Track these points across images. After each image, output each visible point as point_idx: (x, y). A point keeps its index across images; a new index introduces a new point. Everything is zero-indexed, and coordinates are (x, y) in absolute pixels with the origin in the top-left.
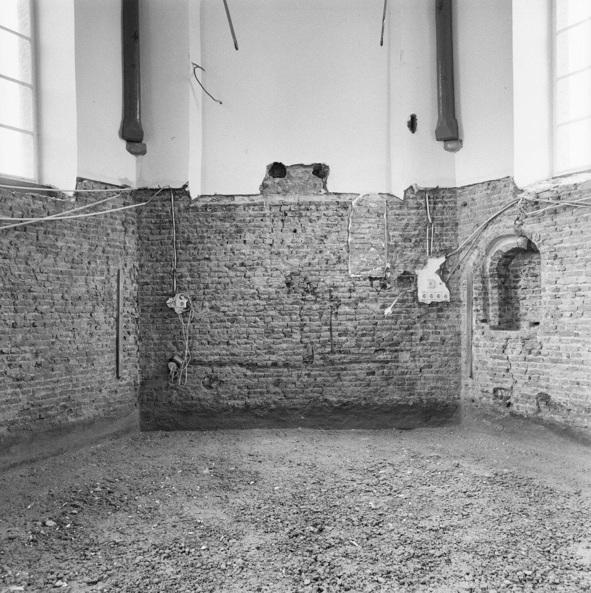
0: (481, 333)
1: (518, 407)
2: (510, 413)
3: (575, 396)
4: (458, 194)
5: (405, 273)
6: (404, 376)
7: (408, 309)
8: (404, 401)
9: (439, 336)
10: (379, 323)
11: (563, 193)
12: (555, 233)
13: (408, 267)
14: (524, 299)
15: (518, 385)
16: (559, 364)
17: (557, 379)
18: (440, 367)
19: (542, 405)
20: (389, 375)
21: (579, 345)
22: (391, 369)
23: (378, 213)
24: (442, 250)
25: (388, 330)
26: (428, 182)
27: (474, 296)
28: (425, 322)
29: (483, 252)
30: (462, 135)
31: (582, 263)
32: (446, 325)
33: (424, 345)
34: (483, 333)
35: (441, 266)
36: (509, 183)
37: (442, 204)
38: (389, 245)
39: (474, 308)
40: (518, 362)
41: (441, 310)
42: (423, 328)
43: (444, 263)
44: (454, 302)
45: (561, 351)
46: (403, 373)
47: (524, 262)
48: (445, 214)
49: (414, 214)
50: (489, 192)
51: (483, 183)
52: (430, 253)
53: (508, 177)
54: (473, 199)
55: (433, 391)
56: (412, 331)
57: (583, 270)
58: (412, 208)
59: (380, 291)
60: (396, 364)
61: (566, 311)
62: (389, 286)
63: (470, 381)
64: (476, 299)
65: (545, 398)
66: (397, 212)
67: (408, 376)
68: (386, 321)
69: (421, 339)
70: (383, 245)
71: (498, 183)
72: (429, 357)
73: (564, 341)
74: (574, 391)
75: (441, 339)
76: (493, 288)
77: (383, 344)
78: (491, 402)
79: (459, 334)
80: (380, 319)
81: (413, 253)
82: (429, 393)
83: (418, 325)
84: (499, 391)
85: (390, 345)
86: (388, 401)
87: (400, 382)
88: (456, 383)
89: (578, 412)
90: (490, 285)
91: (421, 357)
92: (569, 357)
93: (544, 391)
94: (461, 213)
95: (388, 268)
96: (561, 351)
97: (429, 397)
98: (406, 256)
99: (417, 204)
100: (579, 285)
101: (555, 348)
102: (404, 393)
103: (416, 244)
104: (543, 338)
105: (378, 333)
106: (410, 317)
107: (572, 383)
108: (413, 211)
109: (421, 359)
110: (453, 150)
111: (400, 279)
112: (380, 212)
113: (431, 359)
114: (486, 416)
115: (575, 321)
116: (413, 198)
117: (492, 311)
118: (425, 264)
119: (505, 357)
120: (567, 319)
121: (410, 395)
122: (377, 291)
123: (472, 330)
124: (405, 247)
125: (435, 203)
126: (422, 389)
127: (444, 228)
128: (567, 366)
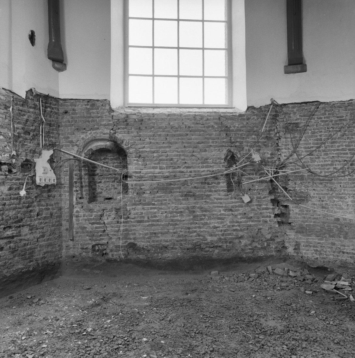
0: (81, 207)
1: (112, 255)
2: (106, 260)
3: (153, 241)
4: (60, 104)
5: (27, 160)
6: (26, 247)
7: (28, 191)
8: (27, 268)
9: (49, 212)
10: (7, 204)
11: (145, 118)
12: (140, 142)
13: (28, 156)
14: (100, 182)
15: (112, 240)
16: (142, 224)
17: (141, 232)
18: (50, 235)
19: (130, 251)
20: (15, 248)
21: (156, 210)
22: (16, 242)
23: (6, 105)
24: (50, 145)
25: (14, 209)
26: (43, 89)
27: (75, 180)
28: (39, 201)
29: (81, 149)
30: (67, 61)
31: (157, 162)
32: (53, 203)
33: (39, 219)
34: (82, 207)
35: (50, 157)
36: (106, 104)
37: (50, 108)
38: (14, 135)
39: (74, 189)
40: (112, 225)
41: (49, 191)
42: (38, 205)
43: (52, 155)
44: (58, 185)
45: (143, 215)
46: (25, 245)
47: (101, 158)
48: (52, 117)
49: (33, 113)
50: (88, 107)
51: (84, 100)
52: (42, 145)
53: (106, 100)
54: (73, 110)
55: (46, 255)
56: (30, 209)
57: (158, 166)
58: (31, 107)
59: (7, 175)
60: (20, 238)
61: (146, 190)
62: (14, 171)
63: (71, 243)
64: (76, 182)
65: (133, 246)
66: (21, 108)
67: (29, 247)
68: (12, 201)
69: (38, 215)
70: (10, 134)
71: (96, 102)
72: (43, 228)
73: (146, 209)
74: (153, 239)
75: (50, 213)
76: (85, 174)
77: (10, 221)
78: (90, 255)
79: (60, 209)
80: (8, 200)
81: (32, 145)
82: (43, 257)
83: (35, 204)
84: (97, 246)
85: (15, 222)
86: (15, 271)
87: (23, 253)
88: (59, 246)
89: (155, 251)
90: (83, 173)
91: (37, 229)
92: (148, 218)
93: (132, 241)
94: (62, 118)
95: (14, 155)
96: (143, 215)
97: (43, 260)
98: (26, 147)
99: (34, 105)
100: (155, 175)
101: (140, 213)
102: (26, 261)
103: (33, 137)
104: (131, 207)
105: (7, 212)
106: (30, 197)
107: (151, 233)
108: (31, 110)
109: (37, 231)
110: (59, 70)
111: (22, 166)
112: (8, 105)
113: (44, 230)
114: (85, 266)
115: (153, 196)
116: (31, 99)
117: (85, 191)
118: (40, 154)
119: (102, 222)
120: (147, 195)
121: (31, 261)
122: (6, 175)
123: (73, 205)
124: (26, 139)
125: (46, 107)
126: (38, 255)
127: (51, 128)
128: (148, 224)
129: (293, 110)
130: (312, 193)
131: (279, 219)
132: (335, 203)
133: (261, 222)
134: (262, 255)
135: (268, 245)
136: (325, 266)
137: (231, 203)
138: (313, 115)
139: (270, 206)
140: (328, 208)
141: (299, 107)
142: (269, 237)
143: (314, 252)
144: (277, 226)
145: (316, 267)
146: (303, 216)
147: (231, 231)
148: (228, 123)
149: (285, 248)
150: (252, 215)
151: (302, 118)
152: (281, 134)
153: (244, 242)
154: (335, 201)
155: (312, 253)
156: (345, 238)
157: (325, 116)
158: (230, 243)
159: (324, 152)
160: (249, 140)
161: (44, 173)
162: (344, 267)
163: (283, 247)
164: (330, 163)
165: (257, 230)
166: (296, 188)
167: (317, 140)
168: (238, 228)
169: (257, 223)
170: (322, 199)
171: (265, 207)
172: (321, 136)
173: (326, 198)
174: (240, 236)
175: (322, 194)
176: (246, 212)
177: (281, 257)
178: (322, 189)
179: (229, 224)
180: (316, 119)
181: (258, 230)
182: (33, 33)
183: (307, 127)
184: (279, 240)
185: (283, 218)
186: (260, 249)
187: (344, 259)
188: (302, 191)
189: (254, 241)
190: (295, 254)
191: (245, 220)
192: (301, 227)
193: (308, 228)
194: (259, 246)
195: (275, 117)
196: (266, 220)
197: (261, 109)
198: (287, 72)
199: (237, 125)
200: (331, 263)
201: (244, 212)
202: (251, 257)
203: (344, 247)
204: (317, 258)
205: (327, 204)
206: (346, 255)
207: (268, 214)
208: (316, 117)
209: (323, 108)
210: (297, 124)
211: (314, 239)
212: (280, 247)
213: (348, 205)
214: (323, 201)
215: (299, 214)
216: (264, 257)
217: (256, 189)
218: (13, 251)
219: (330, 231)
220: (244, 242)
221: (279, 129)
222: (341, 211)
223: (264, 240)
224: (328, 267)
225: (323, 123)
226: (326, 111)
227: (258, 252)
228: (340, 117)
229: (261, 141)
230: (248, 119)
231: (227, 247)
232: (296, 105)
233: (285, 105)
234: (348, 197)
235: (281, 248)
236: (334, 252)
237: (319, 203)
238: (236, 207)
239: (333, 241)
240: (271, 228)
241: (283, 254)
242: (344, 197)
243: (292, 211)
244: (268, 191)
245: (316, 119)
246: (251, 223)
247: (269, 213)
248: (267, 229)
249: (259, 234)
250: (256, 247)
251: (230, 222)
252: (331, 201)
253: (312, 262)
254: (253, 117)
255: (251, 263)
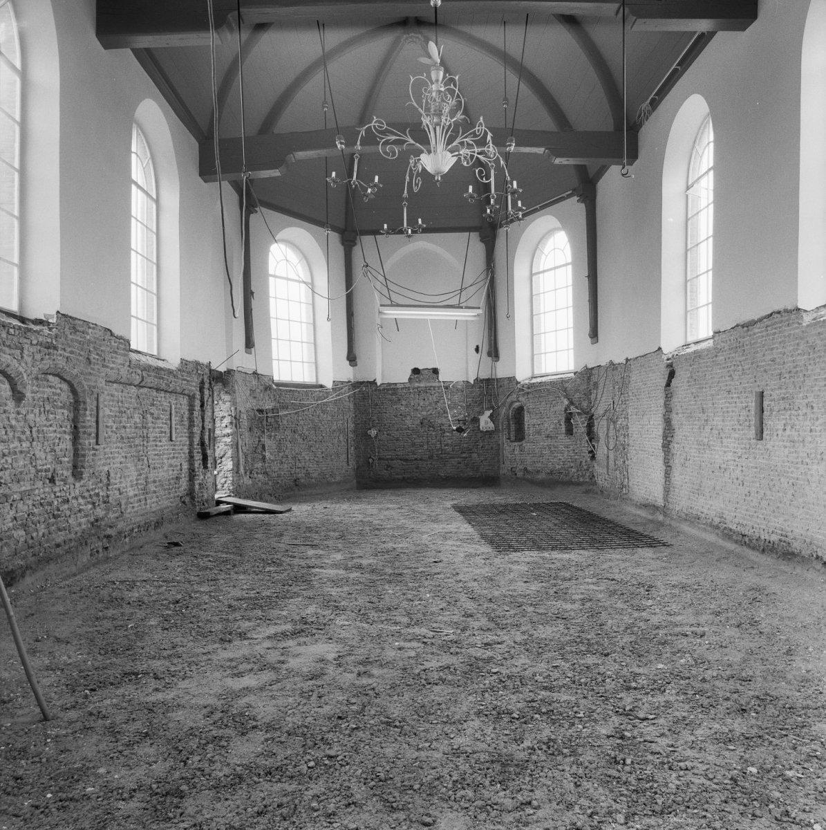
44: (496, 430)
161: (485, 422)
182: (477, 346)
218: (467, 465)
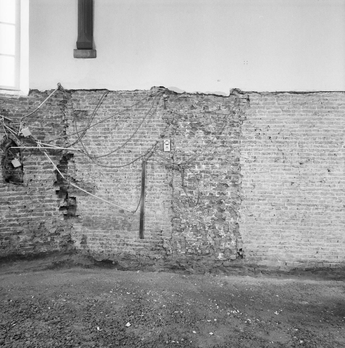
129: (82, 96)
130: (99, 184)
131: (65, 212)
132: (120, 195)
133: (44, 216)
134: (44, 251)
135: (52, 240)
136: (110, 259)
137: (7, 196)
138: (101, 103)
139: (55, 198)
140: (113, 200)
141: (89, 94)
142: (53, 231)
143: (99, 245)
144: (62, 219)
145: (101, 260)
146: (90, 208)
147: (8, 226)
148: (7, 106)
149: (71, 242)
150: (34, 208)
151: (91, 106)
152: (69, 121)
153: (22, 238)
154: (119, 193)
155: (98, 247)
156: (129, 230)
157: (113, 105)
158: (6, 239)
159: (111, 143)
160: (31, 126)
162: (128, 259)
163: (70, 241)
164: (116, 154)
165: (39, 224)
166: (84, 179)
167: (105, 129)
168: (16, 222)
169: (39, 217)
170: (108, 190)
171: (49, 199)
172: (108, 125)
173: (112, 190)
174: (18, 231)
175: (108, 185)
176: (25, 205)
177: (67, 252)
178: (108, 180)
179: (5, 219)
180: (104, 107)
181: (41, 224)
183: (94, 116)
184: (65, 234)
185: (70, 210)
186: (42, 245)
187: (127, 251)
188: (90, 182)
189: (35, 236)
190: (82, 248)
191: (25, 213)
192: (88, 220)
193: (94, 221)
194: (42, 242)
195: (64, 103)
196: (50, 213)
197: (47, 93)
198: (76, 57)
199: (18, 109)
200: (115, 256)
201: (23, 205)
202: (32, 253)
203: (127, 239)
204: (103, 251)
205: (112, 195)
206: (129, 247)
207: (53, 207)
208: (104, 105)
209: (111, 97)
210: (86, 111)
211: (100, 232)
212: (66, 241)
213: (132, 196)
214: (109, 193)
215: (86, 206)
216: (47, 253)
217: (39, 179)
219: (116, 223)
220: (24, 237)
221: (67, 116)
222: (125, 203)
223: (47, 234)
224: (112, 260)
225: (110, 112)
226: (113, 100)
227: (40, 248)
228: (127, 107)
229: (45, 128)
230: (31, 103)
231: (3, 244)
232: (86, 92)
233: (74, 91)
234: (132, 189)
235: (67, 243)
236: (119, 244)
237: (105, 195)
238: (14, 199)
239: (117, 234)
240: (56, 221)
241: (69, 248)
242: (128, 188)
243: (79, 203)
244: (53, 182)
245: (104, 107)
246: (32, 217)
247: (54, 205)
248: (51, 222)
249: (42, 228)
250: (37, 242)
251: (7, 216)
252: (116, 192)
253: (98, 256)
254: (37, 101)
255: (32, 260)
